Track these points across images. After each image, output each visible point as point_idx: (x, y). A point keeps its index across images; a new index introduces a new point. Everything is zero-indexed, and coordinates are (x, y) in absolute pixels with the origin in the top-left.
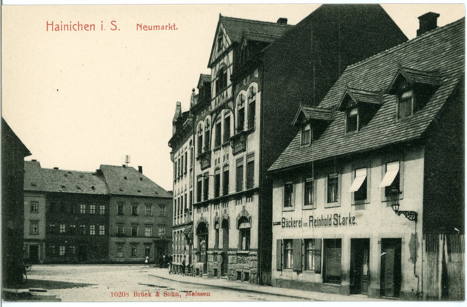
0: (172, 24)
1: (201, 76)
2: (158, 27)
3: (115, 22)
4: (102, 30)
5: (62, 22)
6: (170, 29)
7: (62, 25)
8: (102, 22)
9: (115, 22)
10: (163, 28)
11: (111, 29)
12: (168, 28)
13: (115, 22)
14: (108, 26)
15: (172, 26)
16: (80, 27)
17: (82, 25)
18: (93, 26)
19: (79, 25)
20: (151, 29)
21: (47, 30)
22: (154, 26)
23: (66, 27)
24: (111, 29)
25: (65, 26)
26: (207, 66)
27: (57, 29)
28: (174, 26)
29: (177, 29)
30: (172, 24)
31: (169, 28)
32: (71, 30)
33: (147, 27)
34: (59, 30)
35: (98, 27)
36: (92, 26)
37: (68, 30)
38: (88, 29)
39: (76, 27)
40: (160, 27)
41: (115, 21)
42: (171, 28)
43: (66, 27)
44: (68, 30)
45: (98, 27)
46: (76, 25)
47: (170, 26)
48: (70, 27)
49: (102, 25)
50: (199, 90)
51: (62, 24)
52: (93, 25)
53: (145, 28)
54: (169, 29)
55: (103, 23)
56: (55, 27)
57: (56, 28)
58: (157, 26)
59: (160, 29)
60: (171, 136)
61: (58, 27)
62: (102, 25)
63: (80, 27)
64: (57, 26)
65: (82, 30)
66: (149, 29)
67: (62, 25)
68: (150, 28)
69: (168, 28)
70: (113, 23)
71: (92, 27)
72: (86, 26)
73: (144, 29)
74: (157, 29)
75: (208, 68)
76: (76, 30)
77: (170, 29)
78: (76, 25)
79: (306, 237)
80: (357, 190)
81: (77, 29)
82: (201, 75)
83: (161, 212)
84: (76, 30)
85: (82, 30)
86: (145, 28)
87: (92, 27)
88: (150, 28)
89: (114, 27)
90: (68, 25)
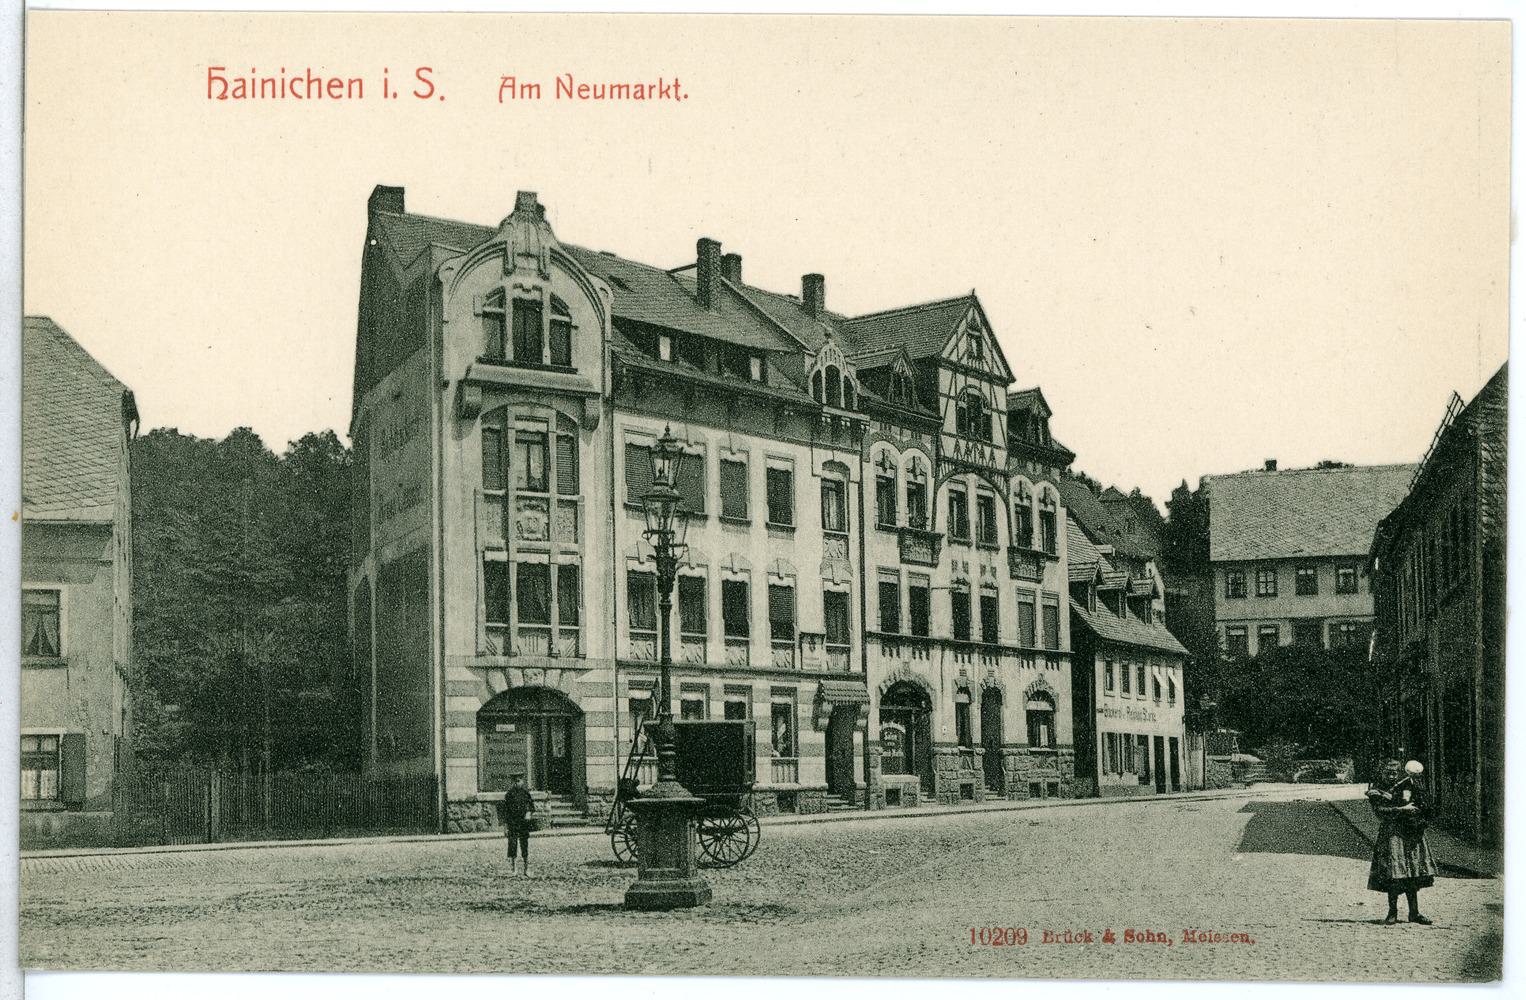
0: (669, 81)
1: (518, 199)
2: (624, 90)
3: (430, 70)
4: (210, 97)
5: (283, 70)
6: (664, 95)
7: (253, 80)
8: (386, 71)
9: (430, 70)
10: (639, 94)
11: (416, 93)
12: (656, 92)
13: (427, 72)
14: (405, 83)
15: (669, 87)
16: (314, 86)
17: (319, 80)
18: (270, 83)
19: (309, 82)
20: (603, 96)
21: (501, 101)
22: (612, 87)
23: (269, 86)
24: (416, 93)
25: (264, 82)
27: (239, 93)
28: (677, 86)
29: (686, 96)
30: (669, 81)
31: (661, 93)
32: (283, 96)
33: (341, 86)
34: (244, 95)
35: (373, 87)
36: (265, 85)
37: (274, 96)
38: (299, 94)
39: (300, 88)
40: (632, 90)
41: (428, 66)
42: (666, 91)
43: (269, 86)
44: (274, 96)
45: (373, 87)
46: (301, 80)
47: (664, 88)
48: (276, 87)
49: (386, 80)
50: (490, 233)
51: (387, 76)
52: (269, 80)
53: (332, 90)
54: (661, 97)
55: (388, 76)
56: (632, 90)
57: (236, 90)
58: (620, 87)
59: (631, 96)
60: (201, 434)
61: (244, 87)
62: (386, 80)
63: (314, 86)
64: (240, 83)
65: (320, 96)
66: (596, 97)
67: (253, 80)
68: (599, 93)
69: (656, 92)
70: (424, 74)
71: (355, 86)
72: (335, 83)
73: (330, 93)
74: (530, 96)
75: (705, 246)
76: (300, 97)
77: (664, 95)
78: (301, 80)
80: (850, 315)
81: (305, 95)
82: (519, 193)
83: (521, 776)
84: (300, 97)
85: (320, 96)
86: (332, 90)
87: (355, 86)
88: (599, 93)
89: (424, 89)
90: (273, 81)
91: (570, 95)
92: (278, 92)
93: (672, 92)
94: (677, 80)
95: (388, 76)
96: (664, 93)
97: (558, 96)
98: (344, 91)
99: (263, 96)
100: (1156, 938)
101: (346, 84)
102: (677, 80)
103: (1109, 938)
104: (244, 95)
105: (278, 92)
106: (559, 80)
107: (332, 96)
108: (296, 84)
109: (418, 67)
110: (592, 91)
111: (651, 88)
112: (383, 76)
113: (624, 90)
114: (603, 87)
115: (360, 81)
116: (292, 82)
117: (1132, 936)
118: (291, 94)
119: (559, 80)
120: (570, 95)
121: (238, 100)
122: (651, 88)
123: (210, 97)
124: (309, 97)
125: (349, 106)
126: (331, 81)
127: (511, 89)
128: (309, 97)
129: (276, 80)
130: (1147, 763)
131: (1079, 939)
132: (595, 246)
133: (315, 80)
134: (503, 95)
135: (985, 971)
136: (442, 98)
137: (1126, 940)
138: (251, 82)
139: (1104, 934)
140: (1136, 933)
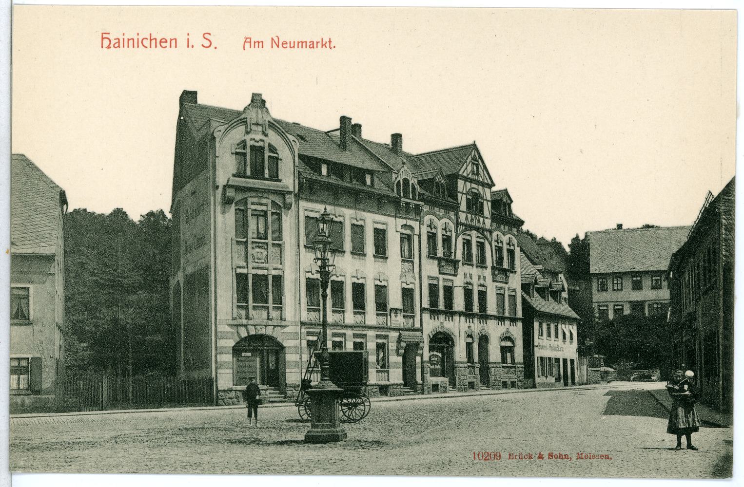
0: (326, 40)
1: (253, 97)
2: (304, 44)
3: (210, 34)
4: (102, 47)
5: (138, 34)
6: (324, 46)
7: (124, 39)
8: (188, 34)
9: (210, 34)
10: (312, 46)
11: (203, 46)
12: (320, 45)
13: (208, 35)
14: (197, 40)
15: (326, 42)
16: (153, 42)
17: (156, 39)
18: (132, 40)
19: (151, 40)
20: (294, 47)
21: (244, 49)
22: (298, 43)
23: (131, 42)
24: (203, 46)
25: (129, 40)
26: (198, 92)
27: (117, 45)
28: (330, 42)
29: (334, 47)
30: (326, 40)
31: (322, 45)
32: (138, 47)
33: (166, 42)
34: (119, 46)
35: (182, 42)
36: (129, 41)
37: (133, 47)
38: (146, 46)
39: (146, 43)
40: (308, 44)
41: (209, 32)
42: (325, 45)
43: (131, 42)
44: (133, 47)
45: (182, 42)
46: (147, 39)
47: (324, 43)
48: (134, 42)
49: (188, 39)
51: (189, 37)
52: (131, 39)
53: (162, 44)
54: (322, 47)
55: (189, 37)
56: (308, 44)
57: (115, 44)
58: (302, 42)
59: (308, 47)
61: (119, 42)
62: (188, 39)
63: (153, 42)
64: (117, 41)
65: (156, 47)
66: (290, 47)
67: (124, 39)
68: (292, 45)
69: (320, 45)
70: (206, 36)
71: (173, 42)
72: (163, 40)
73: (161, 45)
74: (259, 47)
76: (146, 47)
77: (324, 46)
78: (147, 39)
79: (8, 188)
81: (149, 46)
82: (253, 94)
84: (146, 47)
85: (156, 47)
86: (162, 44)
87: (173, 42)
88: (292, 45)
89: (207, 43)
90: (133, 40)
91: (278, 46)
92: (136, 45)
93: (328, 45)
94: (330, 39)
95: (189, 37)
96: (323, 45)
97: (272, 47)
98: (168, 44)
99: (128, 47)
100: (564, 457)
101: (169, 41)
102: (330, 39)
103: (541, 457)
104: (119, 46)
105: (136, 45)
106: (272, 39)
107: (162, 47)
108: (144, 41)
109: (204, 33)
110: (289, 44)
111: (317, 43)
112: (187, 37)
113: (304, 44)
114: (294, 42)
115: (176, 39)
116: (143, 40)
117: (552, 456)
118: (142, 46)
119: (272, 39)
120: (278, 46)
121: (116, 49)
122: (317, 43)
123: (102, 47)
124: (151, 47)
125: (170, 52)
126: (162, 39)
127: (249, 43)
128: (151, 47)
129: (135, 39)
130: (559, 371)
131: (526, 457)
132: (290, 120)
133: (153, 39)
134: (245, 46)
135: (480, 473)
136: (216, 48)
137: (549, 458)
138: (122, 40)
139: (538, 455)
140: (554, 454)
